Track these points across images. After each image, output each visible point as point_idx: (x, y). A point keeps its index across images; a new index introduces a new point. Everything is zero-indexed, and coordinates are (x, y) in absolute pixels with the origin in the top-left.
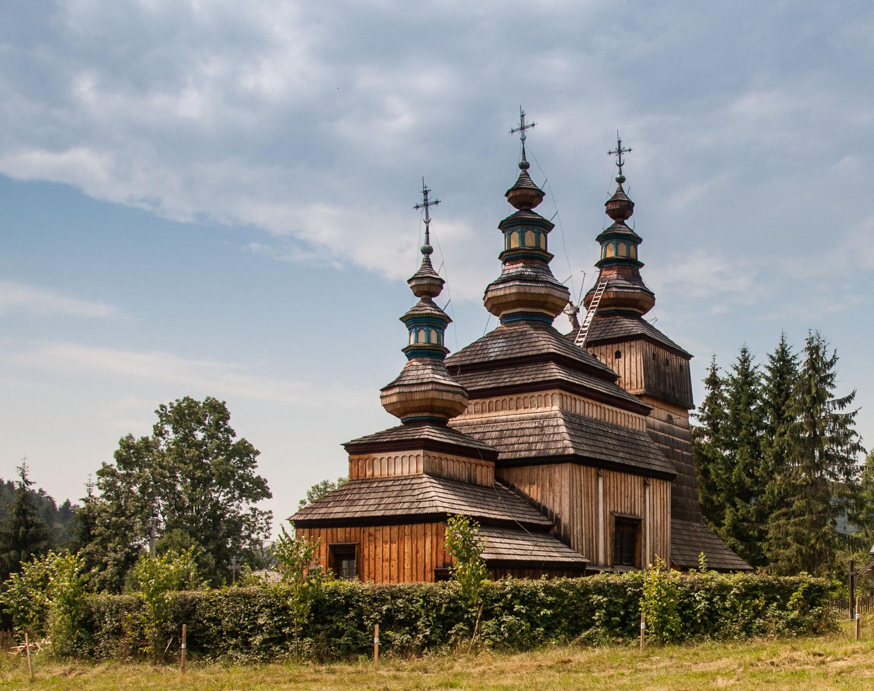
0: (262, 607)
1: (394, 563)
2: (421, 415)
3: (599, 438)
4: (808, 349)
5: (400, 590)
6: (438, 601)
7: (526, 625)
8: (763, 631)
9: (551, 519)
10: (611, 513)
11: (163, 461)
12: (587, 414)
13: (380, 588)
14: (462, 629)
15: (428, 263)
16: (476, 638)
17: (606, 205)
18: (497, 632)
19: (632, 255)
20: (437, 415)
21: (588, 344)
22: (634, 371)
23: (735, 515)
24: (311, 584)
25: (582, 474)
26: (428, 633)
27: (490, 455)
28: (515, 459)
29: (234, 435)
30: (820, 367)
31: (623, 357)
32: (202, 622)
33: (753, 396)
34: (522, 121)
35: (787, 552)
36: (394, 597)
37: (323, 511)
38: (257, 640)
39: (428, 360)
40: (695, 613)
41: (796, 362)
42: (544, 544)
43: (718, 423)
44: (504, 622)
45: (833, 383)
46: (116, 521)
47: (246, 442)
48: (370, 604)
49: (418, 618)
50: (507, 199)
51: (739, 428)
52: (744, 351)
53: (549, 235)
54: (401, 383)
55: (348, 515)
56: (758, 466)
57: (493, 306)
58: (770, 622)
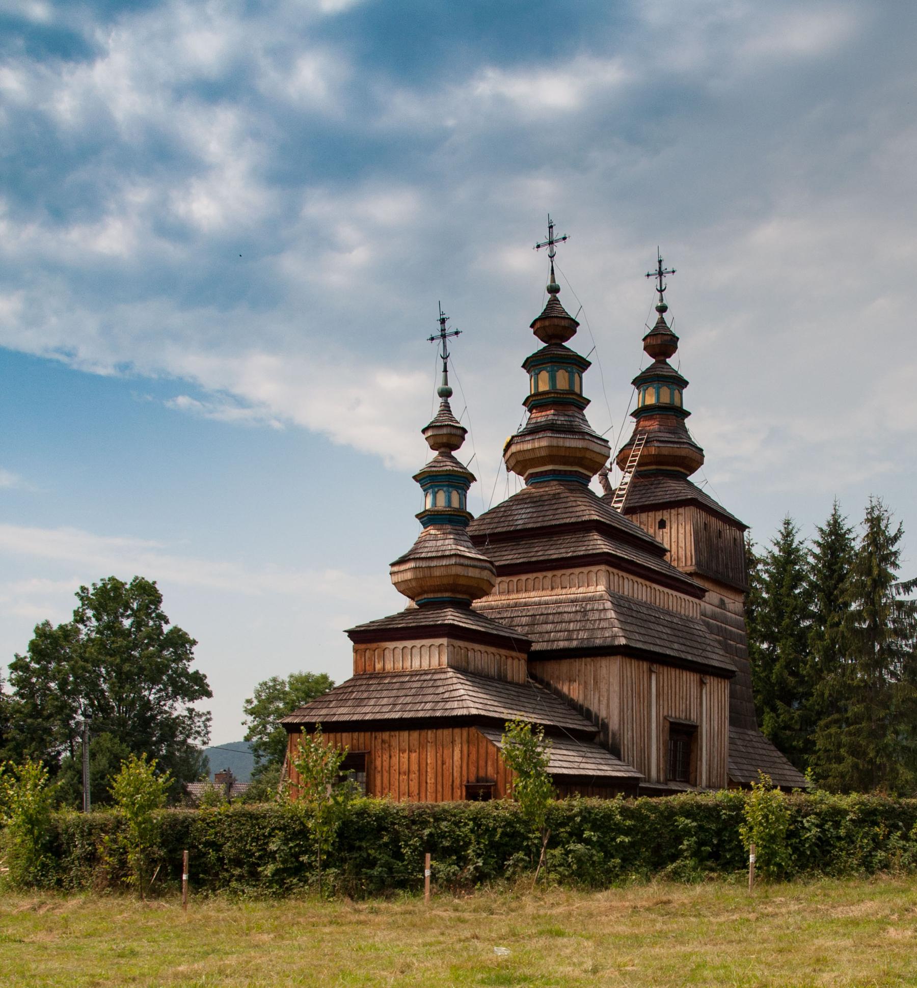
0: (273, 829)
1: (414, 776)
2: (438, 597)
3: (652, 626)
4: (867, 520)
5: (444, 811)
6: (491, 825)
7: (598, 856)
8: (886, 866)
9: (596, 725)
10: (665, 718)
11: (85, 652)
12: (635, 596)
13: (419, 808)
14: (522, 860)
15: (446, 408)
16: (540, 870)
17: (644, 340)
18: (565, 864)
19: (677, 402)
20: (460, 596)
21: (628, 511)
22: (682, 544)
23: (776, 722)
24: (337, 803)
25: (633, 668)
26: (481, 864)
27: (521, 645)
28: (552, 651)
29: (167, 622)
30: (881, 543)
31: (668, 527)
32: (197, 847)
33: (799, 577)
34: (551, 233)
35: (841, 768)
36: (437, 819)
37: (324, 712)
38: (269, 870)
39: (449, 528)
40: (802, 843)
41: (851, 536)
42: (590, 755)
43: (753, 611)
44: (571, 851)
45: (897, 562)
46: (32, 724)
47: (180, 630)
48: (408, 828)
49: (467, 845)
50: (532, 330)
51: (781, 616)
52: (787, 523)
53: (584, 375)
54: (418, 556)
55: (355, 718)
56: (805, 663)
57: (517, 462)
58: (893, 855)
